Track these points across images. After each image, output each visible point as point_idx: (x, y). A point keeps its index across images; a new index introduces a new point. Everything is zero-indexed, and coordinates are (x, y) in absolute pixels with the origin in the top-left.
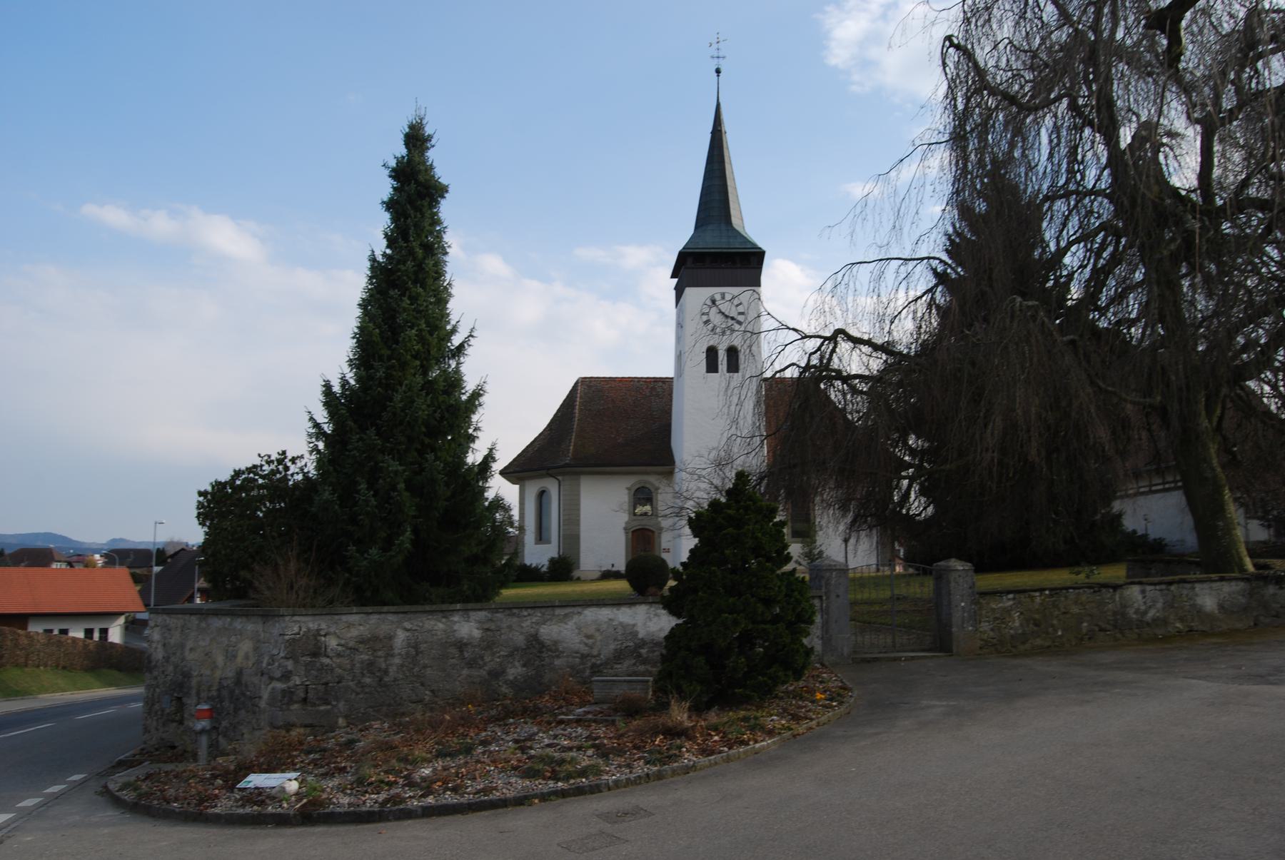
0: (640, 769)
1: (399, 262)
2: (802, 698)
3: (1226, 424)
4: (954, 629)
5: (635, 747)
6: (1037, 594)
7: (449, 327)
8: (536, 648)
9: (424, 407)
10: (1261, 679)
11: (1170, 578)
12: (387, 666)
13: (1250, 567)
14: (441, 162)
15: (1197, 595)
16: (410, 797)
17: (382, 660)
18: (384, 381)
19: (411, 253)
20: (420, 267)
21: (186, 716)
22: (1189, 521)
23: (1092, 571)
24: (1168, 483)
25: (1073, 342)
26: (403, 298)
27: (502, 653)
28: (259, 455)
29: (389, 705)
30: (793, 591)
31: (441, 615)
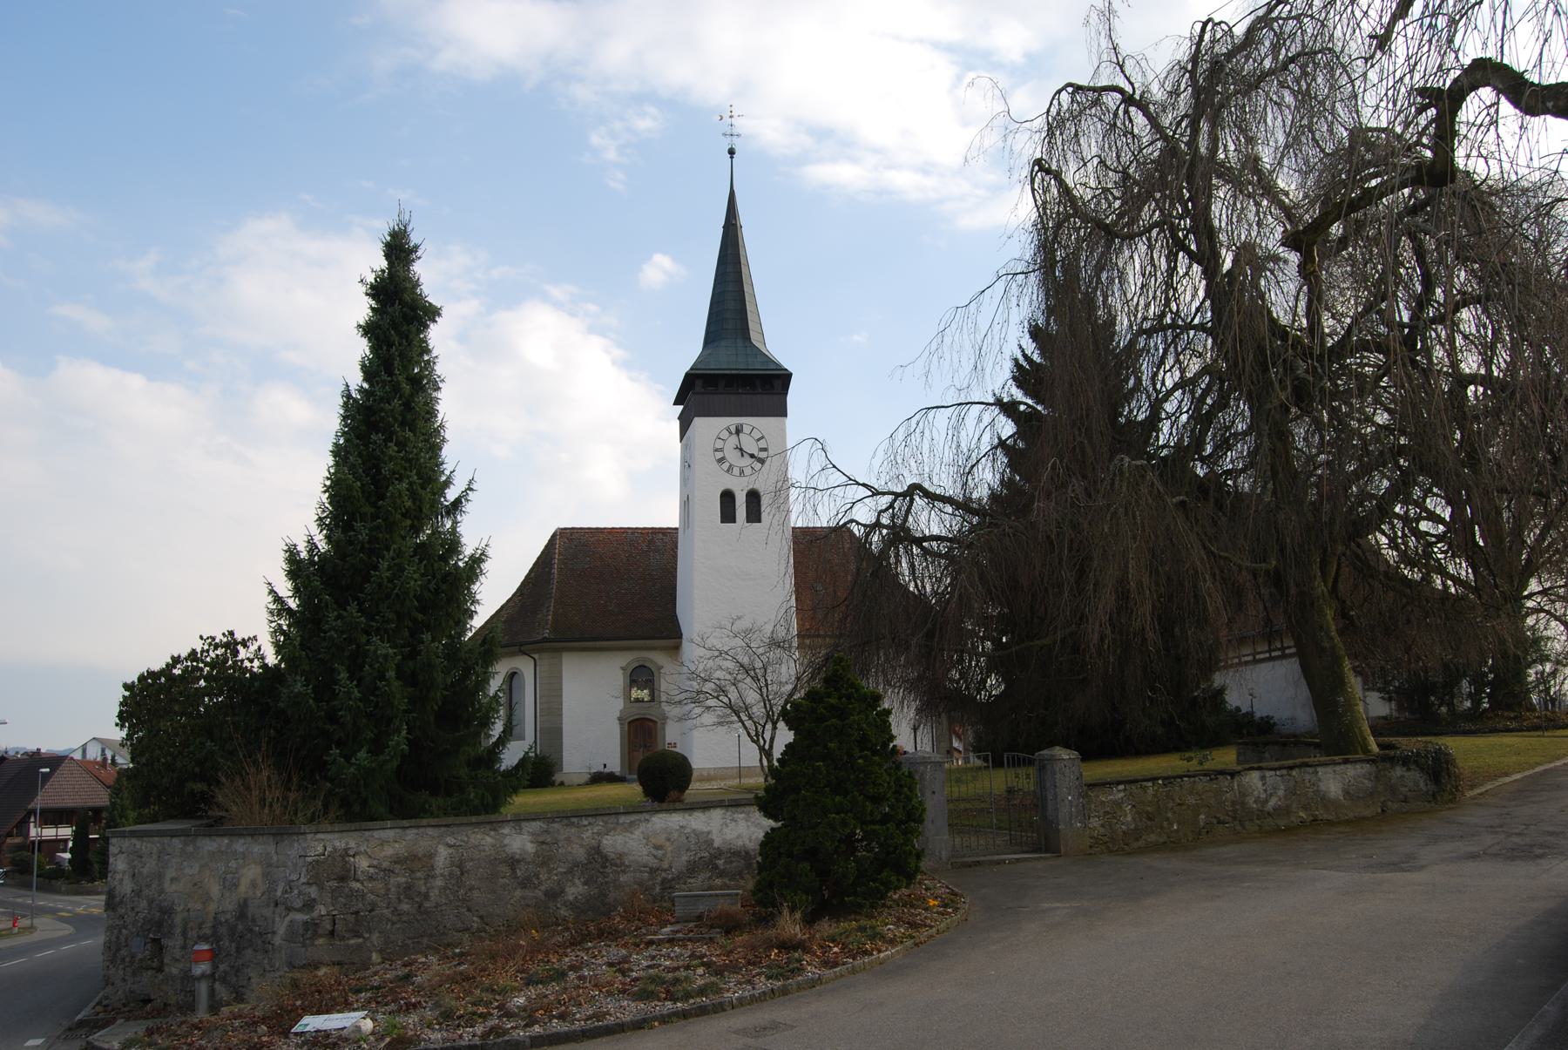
0: (763, 984)
1: (381, 399)
2: (912, 906)
3: (1341, 587)
4: (1061, 827)
5: (749, 963)
6: (1150, 784)
7: (443, 478)
8: (599, 862)
9: (416, 576)
10: (1394, 866)
11: (1290, 762)
12: (428, 889)
13: (1375, 748)
14: (429, 275)
15: (1320, 780)
16: (512, 1028)
17: (422, 882)
18: (367, 546)
19: (396, 389)
20: (408, 406)
21: (165, 961)
22: (1304, 692)
23: (1205, 757)
24: (1274, 650)
25: (1183, 503)
26: (390, 444)
27: (560, 870)
28: (201, 637)
29: (431, 935)
30: (901, 786)
31: (488, 827)
